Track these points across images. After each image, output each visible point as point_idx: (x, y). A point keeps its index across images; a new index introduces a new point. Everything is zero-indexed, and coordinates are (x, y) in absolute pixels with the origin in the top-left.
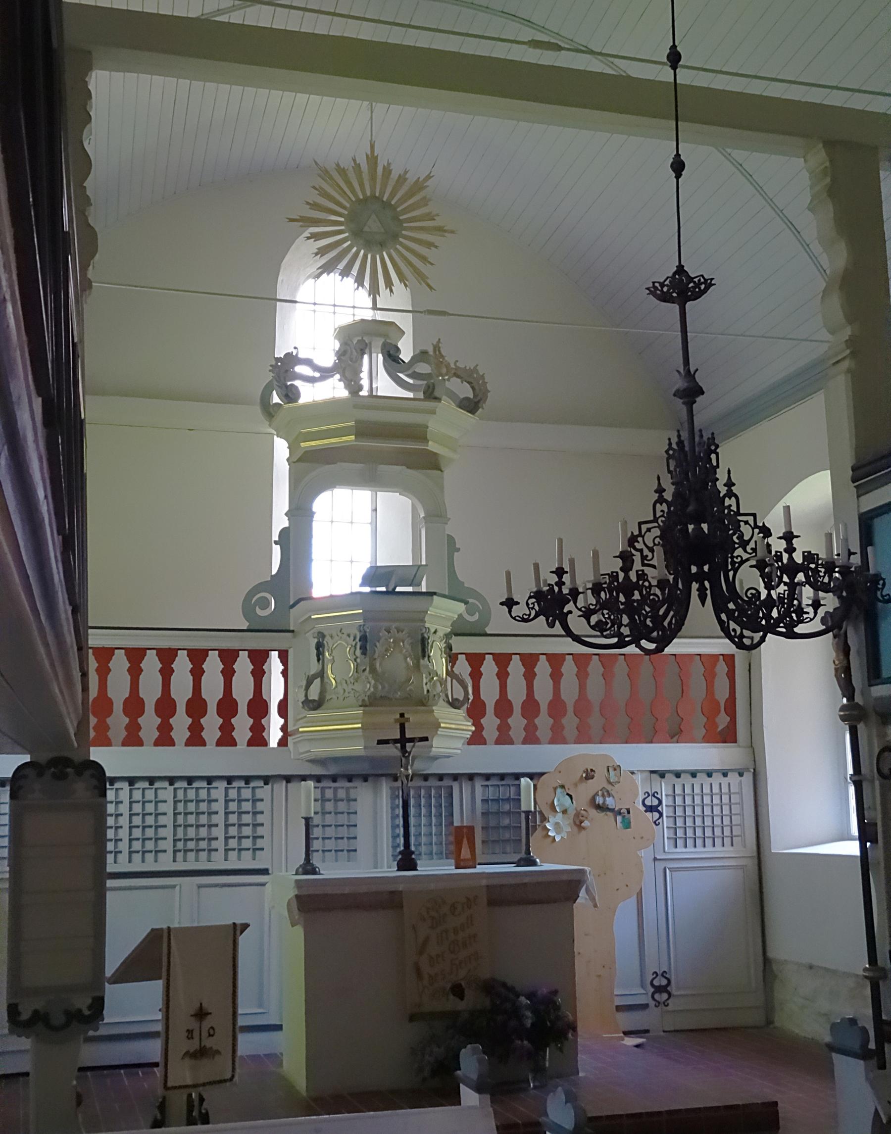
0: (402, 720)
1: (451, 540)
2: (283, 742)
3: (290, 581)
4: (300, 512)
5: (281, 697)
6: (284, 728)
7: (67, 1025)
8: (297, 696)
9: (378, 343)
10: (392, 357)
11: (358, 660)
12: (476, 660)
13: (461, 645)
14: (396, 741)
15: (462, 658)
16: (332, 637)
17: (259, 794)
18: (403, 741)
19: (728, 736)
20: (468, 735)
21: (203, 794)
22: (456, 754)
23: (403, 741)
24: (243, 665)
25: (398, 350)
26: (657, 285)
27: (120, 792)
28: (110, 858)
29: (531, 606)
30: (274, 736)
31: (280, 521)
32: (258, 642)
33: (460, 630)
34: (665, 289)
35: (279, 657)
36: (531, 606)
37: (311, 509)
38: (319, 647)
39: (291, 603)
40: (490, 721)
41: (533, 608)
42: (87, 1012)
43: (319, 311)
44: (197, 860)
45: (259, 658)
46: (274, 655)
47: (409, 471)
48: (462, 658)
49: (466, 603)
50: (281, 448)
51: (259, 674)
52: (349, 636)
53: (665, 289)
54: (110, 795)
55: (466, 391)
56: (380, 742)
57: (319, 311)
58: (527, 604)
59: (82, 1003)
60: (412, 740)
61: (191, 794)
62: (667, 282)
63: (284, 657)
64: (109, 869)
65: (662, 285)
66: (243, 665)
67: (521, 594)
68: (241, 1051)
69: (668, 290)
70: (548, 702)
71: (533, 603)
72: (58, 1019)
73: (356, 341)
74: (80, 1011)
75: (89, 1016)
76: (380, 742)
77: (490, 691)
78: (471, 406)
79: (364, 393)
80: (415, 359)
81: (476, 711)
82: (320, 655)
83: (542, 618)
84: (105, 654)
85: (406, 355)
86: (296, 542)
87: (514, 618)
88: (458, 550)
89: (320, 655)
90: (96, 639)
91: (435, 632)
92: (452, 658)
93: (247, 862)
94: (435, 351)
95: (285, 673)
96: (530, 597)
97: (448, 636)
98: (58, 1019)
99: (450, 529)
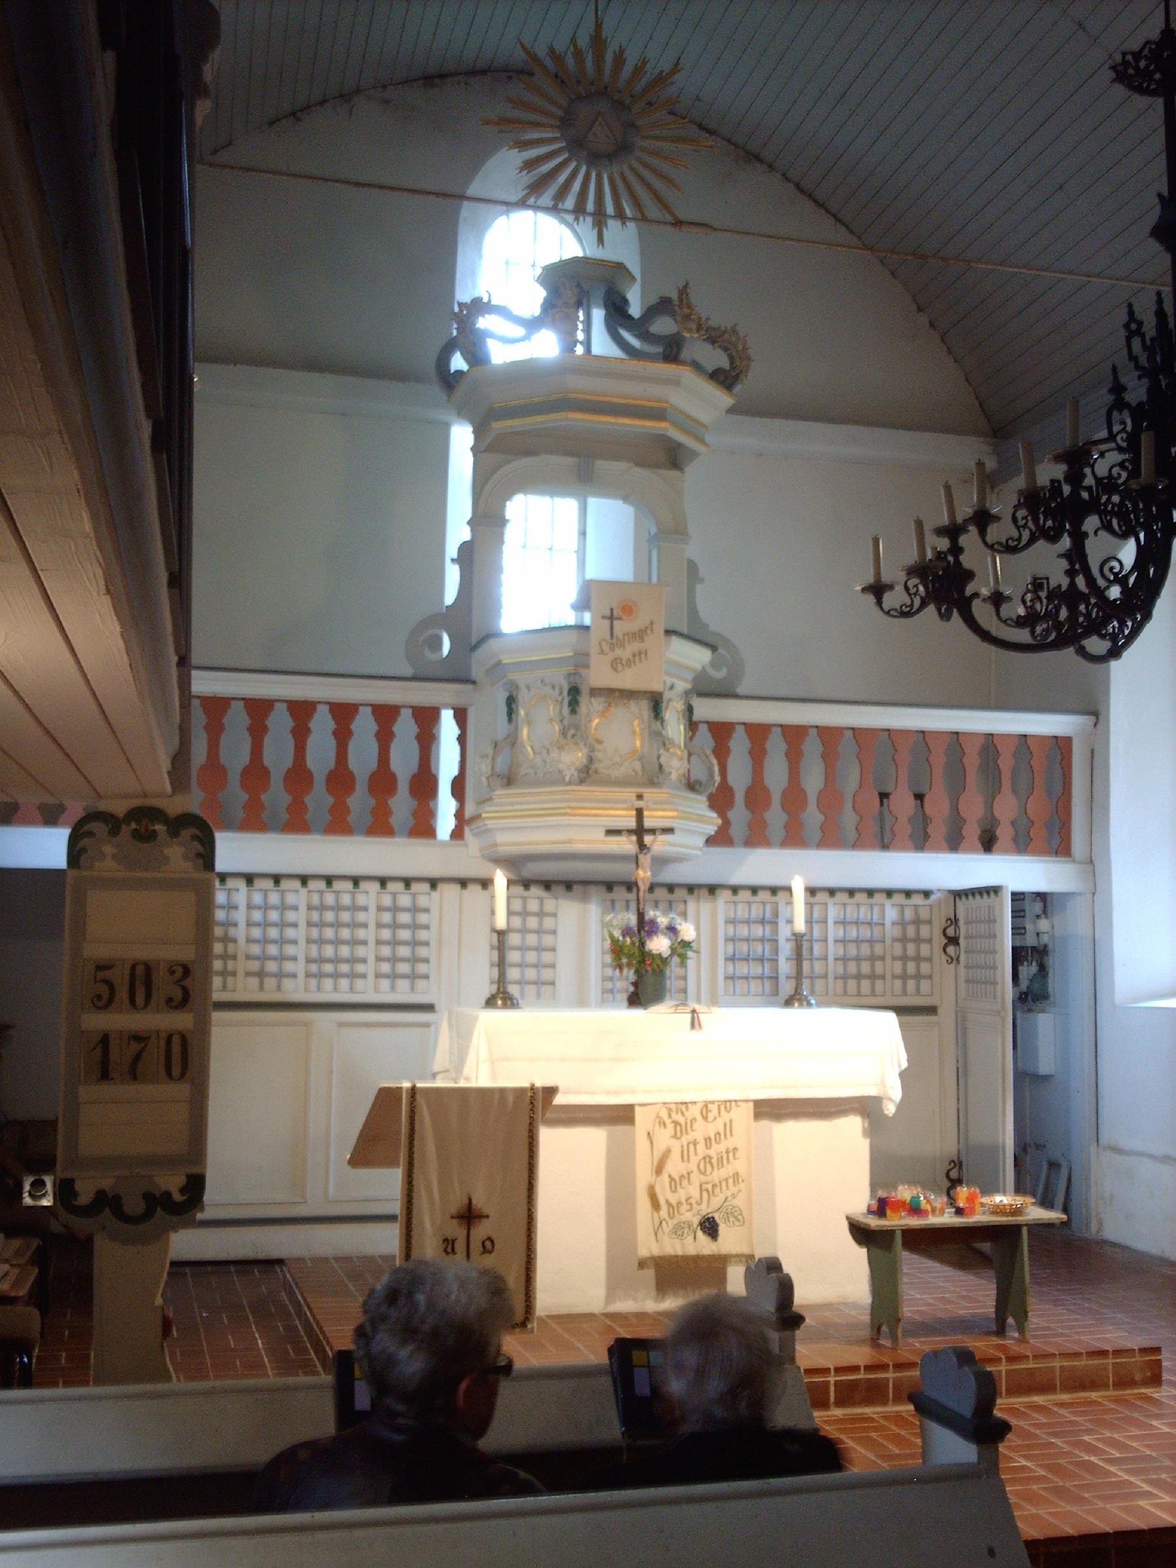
0: (640, 804)
1: (692, 567)
2: (457, 834)
3: (470, 620)
4: (488, 519)
5: (455, 772)
6: (459, 815)
7: (148, 1214)
8: (479, 769)
9: (599, 293)
10: (617, 312)
11: (566, 722)
12: (721, 731)
13: (707, 710)
14: (630, 832)
15: (703, 728)
16: (528, 688)
17: (422, 901)
18: (640, 831)
19: (1060, 846)
20: (711, 829)
21: (346, 900)
22: (697, 856)
23: (640, 831)
24: (405, 727)
25: (626, 301)
26: (1129, 57)
27: (234, 893)
28: (217, 982)
29: (1023, 523)
30: (445, 823)
31: (458, 532)
32: (423, 694)
33: (705, 688)
34: (1142, 64)
35: (455, 716)
36: (913, 591)
37: (504, 516)
38: (511, 702)
39: (474, 643)
40: (739, 813)
41: (1025, 526)
42: (178, 1197)
43: (514, 259)
44: (336, 989)
45: (427, 719)
46: (447, 716)
47: (637, 469)
48: (703, 728)
49: (714, 648)
50: (462, 437)
51: (427, 739)
52: (553, 688)
53: (1142, 64)
54: (220, 897)
55: (717, 359)
56: (610, 832)
57: (514, 259)
58: (1015, 519)
59: (172, 1183)
60: (653, 831)
61: (257, 898)
62: (1146, 52)
63: (461, 717)
64: (217, 996)
65: (1137, 56)
66: (405, 727)
67: (893, 573)
68: (394, 1177)
69: (1147, 66)
70: (735, 809)
71: (1025, 518)
72: (134, 1205)
73: (570, 287)
74: (168, 1195)
75: (184, 1202)
76: (610, 832)
77: (739, 775)
78: (725, 379)
79: (580, 350)
80: (652, 312)
81: (721, 800)
82: (511, 713)
83: (931, 609)
84: (217, 706)
85: (635, 310)
86: (478, 558)
87: (888, 613)
88: (702, 581)
89: (511, 713)
90: (203, 684)
91: (672, 687)
92: (692, 726)
93: (402, 995)
94: (681, 300)
95: (462, 740)
96: (1016, 508)
97: (687, 693)
98: (134, 1205)
99: (692, 550)
